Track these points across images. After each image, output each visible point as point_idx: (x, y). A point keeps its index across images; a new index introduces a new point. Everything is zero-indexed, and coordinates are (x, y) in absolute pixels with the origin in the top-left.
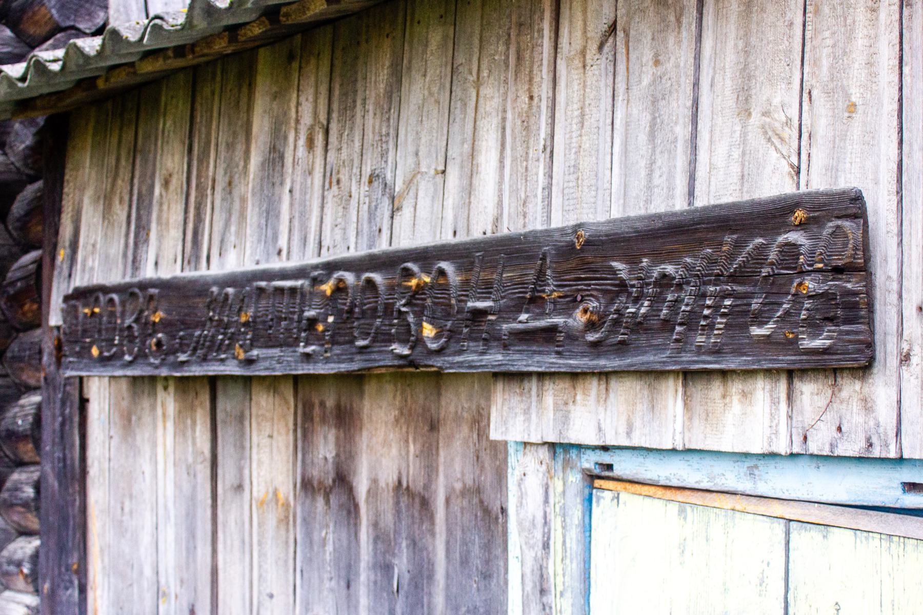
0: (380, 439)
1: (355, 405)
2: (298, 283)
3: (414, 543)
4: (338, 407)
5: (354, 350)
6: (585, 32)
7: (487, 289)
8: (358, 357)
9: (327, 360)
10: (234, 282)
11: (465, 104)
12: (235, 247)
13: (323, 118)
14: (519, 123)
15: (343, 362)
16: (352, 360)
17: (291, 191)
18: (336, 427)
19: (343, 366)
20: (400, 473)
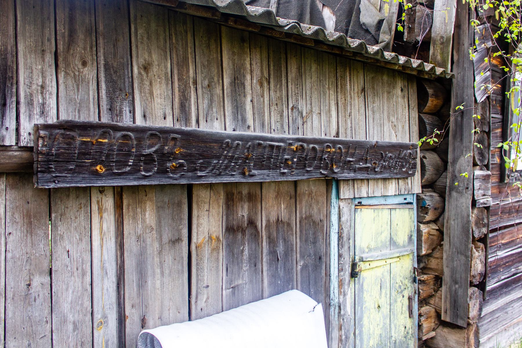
0: (270, 204)
1: (257, 192)
2: (282, 144)
3: (285, 240)
4: (249, 193)
5: (304, 172)
6: (358, 87)
7: (352, 155)
8: (306, 174)
9: (293, 175)
10: (242, 139)
11: (325, 94)
12: (217, 119)
13: (266, 75)
14: (343, 106)
15: (300, 176)
16: (304, 175)
17: (252, 101)
18: (248, 201)
19: (300, 177)
20: (278, 214)
